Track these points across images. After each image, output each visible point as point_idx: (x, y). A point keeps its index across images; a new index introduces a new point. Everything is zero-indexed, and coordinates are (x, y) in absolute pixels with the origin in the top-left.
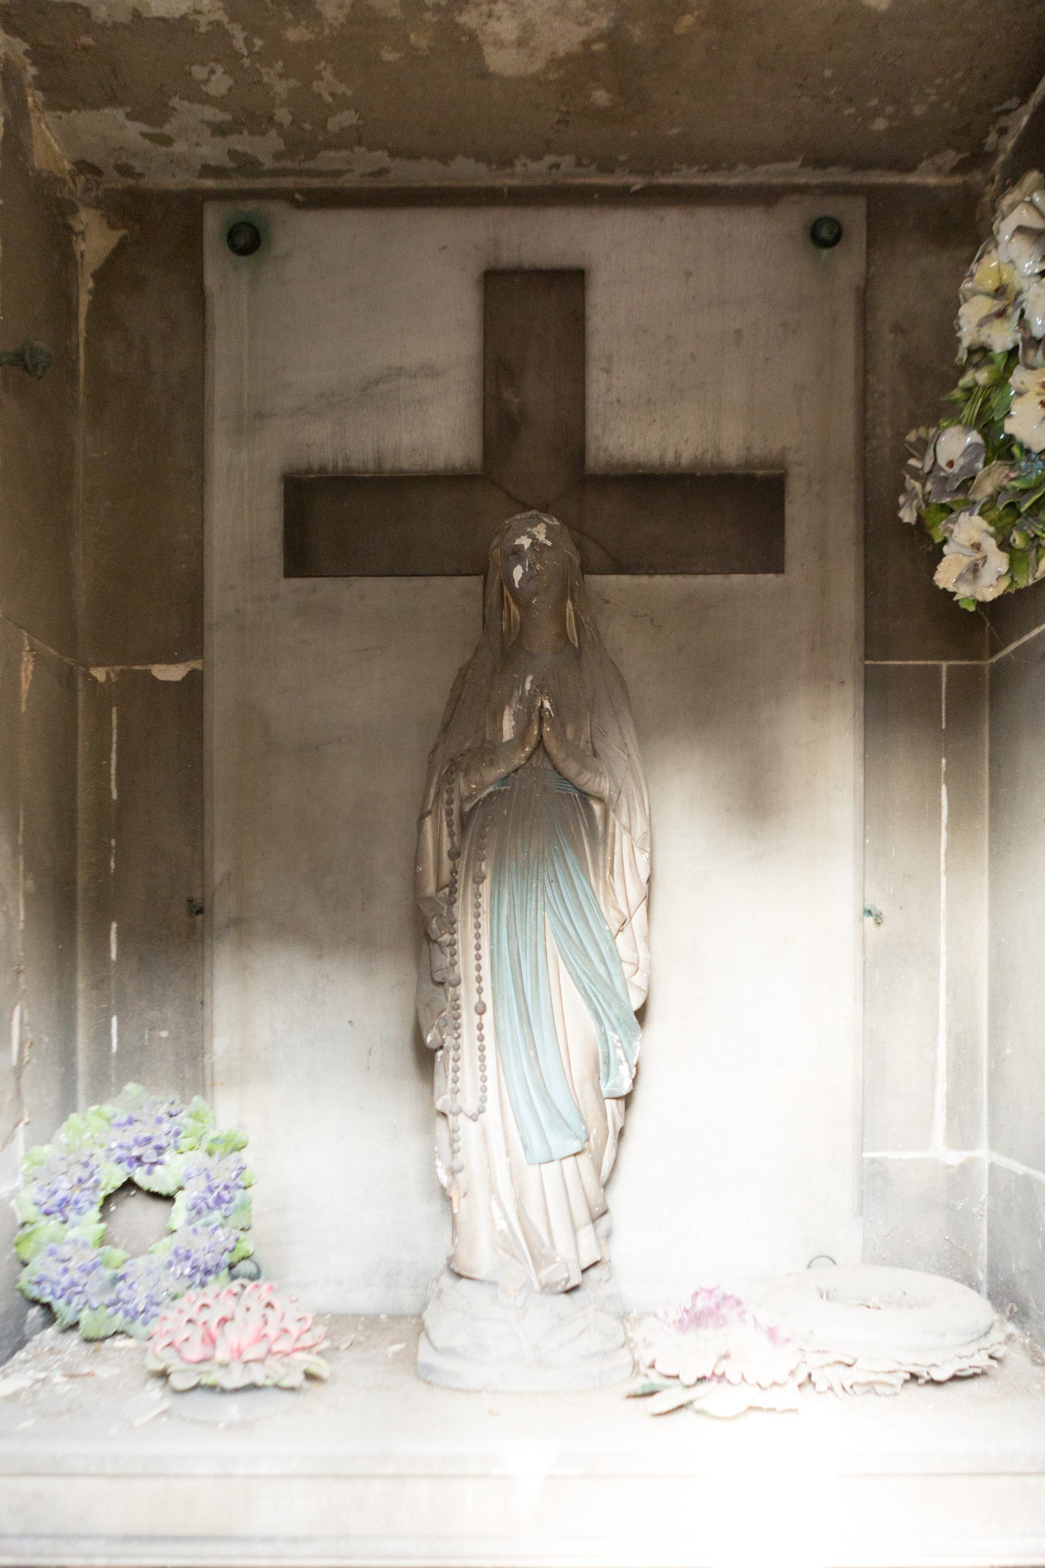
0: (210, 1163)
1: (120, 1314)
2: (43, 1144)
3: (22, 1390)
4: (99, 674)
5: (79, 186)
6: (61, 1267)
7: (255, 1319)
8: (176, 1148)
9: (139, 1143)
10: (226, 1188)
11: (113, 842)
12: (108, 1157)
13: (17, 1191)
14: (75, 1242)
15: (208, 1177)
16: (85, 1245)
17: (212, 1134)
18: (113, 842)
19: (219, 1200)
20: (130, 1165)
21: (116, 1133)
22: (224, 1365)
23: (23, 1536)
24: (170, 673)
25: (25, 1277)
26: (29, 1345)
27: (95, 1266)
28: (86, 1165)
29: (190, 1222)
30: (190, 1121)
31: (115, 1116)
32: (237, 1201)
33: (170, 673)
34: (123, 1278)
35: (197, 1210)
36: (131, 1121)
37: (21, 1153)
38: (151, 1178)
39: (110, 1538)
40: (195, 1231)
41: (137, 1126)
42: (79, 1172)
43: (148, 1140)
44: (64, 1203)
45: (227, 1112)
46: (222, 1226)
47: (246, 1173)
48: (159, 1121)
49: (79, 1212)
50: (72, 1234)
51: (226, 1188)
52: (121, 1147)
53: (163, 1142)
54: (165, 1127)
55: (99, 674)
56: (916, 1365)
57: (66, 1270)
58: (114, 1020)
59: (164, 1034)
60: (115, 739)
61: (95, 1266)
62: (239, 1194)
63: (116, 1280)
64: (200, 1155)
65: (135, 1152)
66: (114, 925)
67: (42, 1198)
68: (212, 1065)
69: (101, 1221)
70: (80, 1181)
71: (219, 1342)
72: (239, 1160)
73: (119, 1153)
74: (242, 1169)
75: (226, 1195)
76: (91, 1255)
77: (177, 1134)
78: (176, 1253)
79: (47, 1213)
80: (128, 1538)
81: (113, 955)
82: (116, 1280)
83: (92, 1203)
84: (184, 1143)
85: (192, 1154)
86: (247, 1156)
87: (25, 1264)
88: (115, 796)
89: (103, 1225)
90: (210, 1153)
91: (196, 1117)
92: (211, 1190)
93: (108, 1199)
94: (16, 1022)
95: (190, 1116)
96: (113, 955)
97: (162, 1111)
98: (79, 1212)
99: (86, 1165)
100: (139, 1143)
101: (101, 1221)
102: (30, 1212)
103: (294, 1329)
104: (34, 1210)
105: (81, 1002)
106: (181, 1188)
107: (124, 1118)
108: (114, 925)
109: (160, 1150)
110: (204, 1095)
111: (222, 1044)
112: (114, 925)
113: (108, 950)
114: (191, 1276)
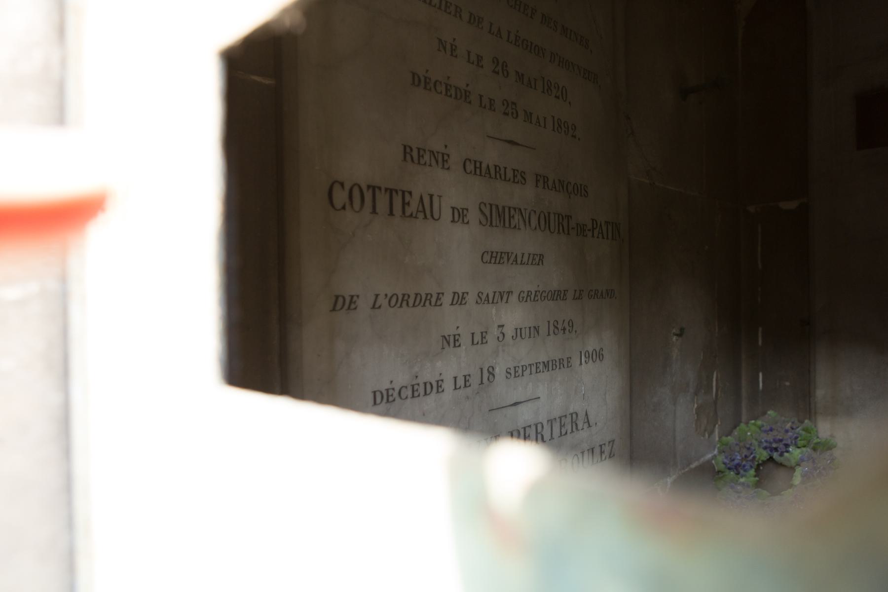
5: (516, 221)
9: (775, 441)
13: (715, 456)
17: (816, 441)
20: (771, 451)
28: (749, 449)
30: (803, 433)
31: (763, 426)
36: (771, 430)
37: (717, 439)
41: (775, 433)
42: (745, 452)
43: (781, 441)
44: (738, 465)
48: (787, 431)
52: (766, 441)
53: (789, 442)
54: (790, 434)
55: (751, 209)
58: (761, 375)
59: (787, 384)
65: (774, 445)
66: (760, 329)
67: (727, 461)
73: (765, 444)
77: (796, 438)
79: (729, 469)
81: (760, 343)
83: (751, 467)
85: (804, 449)
88: (760, 266)
89: (757, 479)
91: (806, 430)
93: (759, 465)
94: (714, 379)
95: (803, 430)
96: (760, 343)
97: (788, 426)
98: (745, 471)
99: (749, 449)
100: (775, 441)
101: (755, 476)
104: (723, 466)
107: (768, 428)
108: (760, 329)
109: (787, 446)
110: (810, 419)
111: (821, 393)
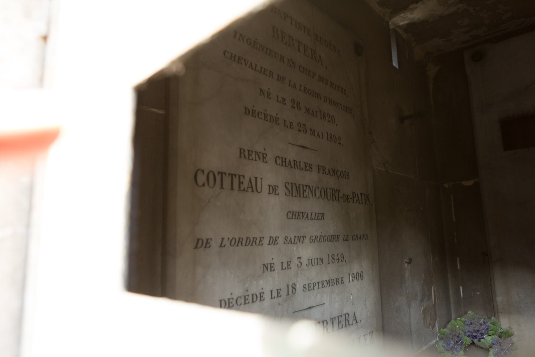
2: (444, 328)
4: (446, 186)
8: (488, 334)
9: (474, 331)
11: (455, 234)
12: (465, 334)
17: (500, 331)
18: (455, 234)
21: (467, 327)
23: (275, 120)
24: (469, 183)
28: (458, 337)
30: (492, 325)
33: (469, 183)
36: (471, 324)
38: (480, 343)
41: (474, 326)
42: (456, 339)
43: (478, 331)
48: (481, 325)
52: (469, 332)
53: (483, 332)
56: (299, 50)
58: (461, 288)
59: (478, 293)
60: (453, 204)
65: (474, 334)
68: (497, 306)
70: (457, 342)
72: (511, 340)
74: (513, 343)
77: (488, 329)
81: (459, 267)
85: (493, 336)
91: (494, 324)
95: (491, 323)
96: (459, 267)
97: (482, 321)
99: (458, 337)
100: (474, 331)
105: (450, 281)
106: (491, 347)
109: (482, 334)
112: (458, 259)
113: (457, 266)
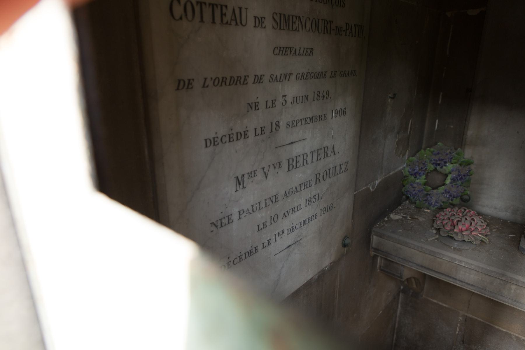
0: (460, 168)
1: (427, 203)
3: (400, 219)
6: (413, 189)
7: (468, 223)
10: (464, 176)
12: (430, 162)
14: (418, 183)
15: (459, 172)
16: (420, 184)
17: (463, 160)
19: (461, 178)
22: (456, 233)
24: (473, 12)
25: (403, 189)
26: (402, 204)
27: (422, 190)
28: (424, 164)
29: (451, 183)
30: (456, 155)
32: (467, 179)
33: (473, 12)
34: (429, 195)
35: (453, 180)
36: (438, 154)
39: (417, 265)
40: (452, 186)
41: (440, 155)
42: (421, 166)
43: (442, 160)
45: (468, 153)
46: (461, 186)
47: (471, 172)
48: (447, 154)
49: (420, 176)
50: (417, 181)
51: (464, 176)
52: (434, 160)
54: (448, 156)
57: (414, 190)
58: (437, 121)
59: (452, 127)
61: (422, 190)
62: (467, 177)
63: (427, 195)
64: (457, 165)
65: (438, 162)
69: (425, 179)
71: (456, 227)
73: (433, 162)
75: (464, 177)
76: (422, 187)
77: (452, 158)
78: (446, 191)
79: (411, 175)
80: (422, 266)
82: (427, 195)
84: (453, 161)
85: (455, 164)
86: (472, 167)
87: (404, 186)
90: (461, 165)
91: (458, 154)
92: (459, 176)
95: (456, 154)
97: (448, 151)
98: (420, 176)
99: (424, 164)
100: (439, 160)
102: (407, 173)
103: (480, 229)
109: (446, 162)
110: (461, 148)
114: (449, 198)
